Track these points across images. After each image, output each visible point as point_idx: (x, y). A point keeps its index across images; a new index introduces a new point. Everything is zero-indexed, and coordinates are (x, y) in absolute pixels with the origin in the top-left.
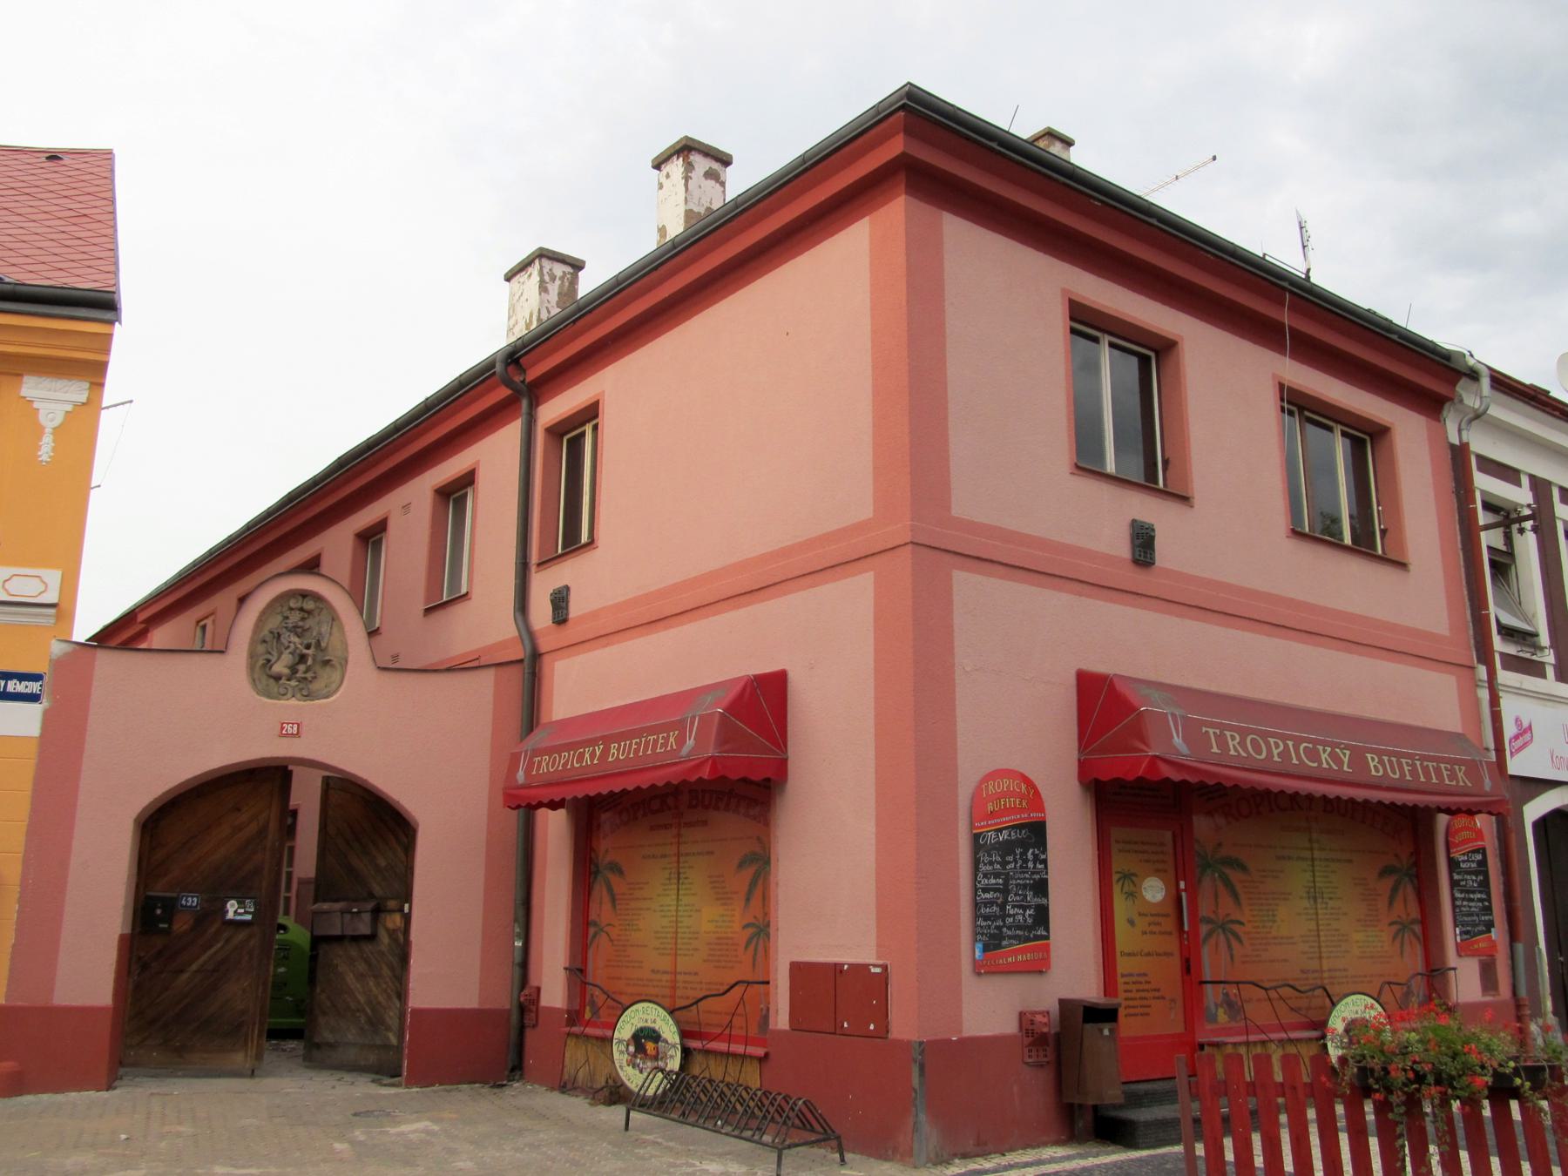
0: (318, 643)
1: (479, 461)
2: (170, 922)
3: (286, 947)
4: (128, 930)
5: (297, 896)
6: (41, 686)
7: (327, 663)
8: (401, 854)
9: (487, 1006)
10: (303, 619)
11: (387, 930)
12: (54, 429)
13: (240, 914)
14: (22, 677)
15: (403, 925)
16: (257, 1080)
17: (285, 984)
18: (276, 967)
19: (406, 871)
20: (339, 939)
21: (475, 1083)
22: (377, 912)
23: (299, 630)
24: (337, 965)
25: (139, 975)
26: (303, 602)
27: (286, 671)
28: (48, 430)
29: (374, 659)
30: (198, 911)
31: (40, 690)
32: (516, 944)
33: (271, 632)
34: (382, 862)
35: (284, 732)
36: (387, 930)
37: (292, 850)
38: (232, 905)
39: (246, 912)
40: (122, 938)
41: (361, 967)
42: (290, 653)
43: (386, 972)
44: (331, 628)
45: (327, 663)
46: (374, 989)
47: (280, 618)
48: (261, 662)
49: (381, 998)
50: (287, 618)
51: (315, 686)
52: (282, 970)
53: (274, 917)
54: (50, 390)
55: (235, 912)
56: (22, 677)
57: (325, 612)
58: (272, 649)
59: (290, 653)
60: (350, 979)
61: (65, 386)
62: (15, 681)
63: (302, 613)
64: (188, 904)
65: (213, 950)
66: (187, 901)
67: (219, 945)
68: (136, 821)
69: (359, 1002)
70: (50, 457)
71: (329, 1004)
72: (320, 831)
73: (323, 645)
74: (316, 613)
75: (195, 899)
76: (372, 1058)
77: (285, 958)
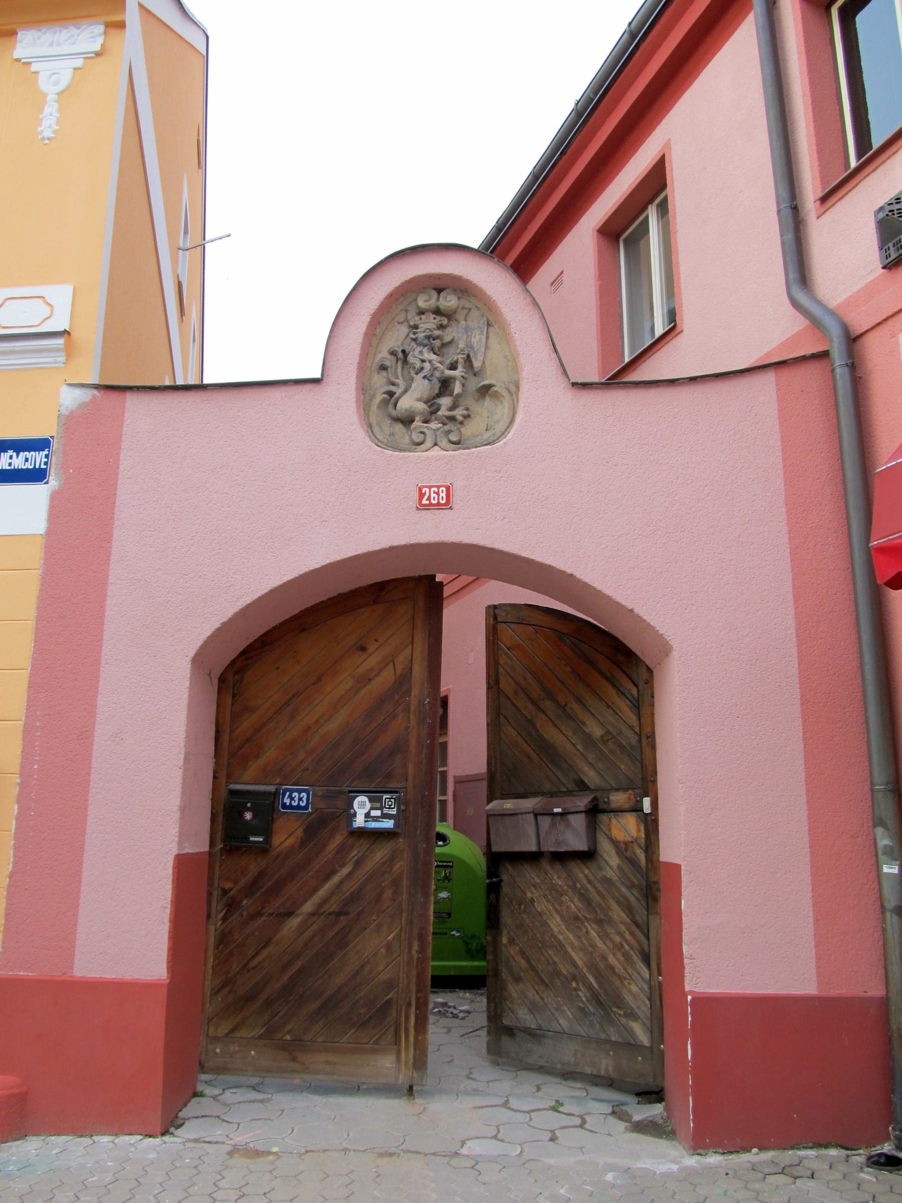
0: (468, 360)
1: (669, 140)
2: (267, 832)
3: (447, 864)
4: (200, 844)
5: (454, 796)
6: (47, 456)
7: (485, 391)
8: (632, 718)
9: (834, 992)
10: (441, 327)
11: (615, 843)
12: (58, 94)
13: (376, 819)
14: (20, 446)
15: (643, 835)
16: (419, 1101)
17: (449, 915)
18: (438, 889)
19: (640, 741)
20: (534, 857)
21: (826, 1146)
22: (594, 811)
23: (437, 343)
24: (532, 901)
25: (224, 919)
26: (438, 299)
27: (421, 406)
28: (52, 97)
29: (565, 372)
30: (310, 814)
31: (46, 463)
32: (886, 869)
33: (393, 353)
34: (597, 732)
35: (424, 501)
36: (615, 843)
37: (444, 746)
38: (362, 805)
39: (385, 816)
40: (183, 863)
41: (574, 905)
42: (424, 377)
43: (618, 913)
44: (487, 338)
45: (485, 391)
46: (600, 943)
47: (404, 329)
48: (379, 397)
49: (612, 960)
50: (416, 327)
51: (469, 429)
52: (444, 895)
53: (430, 824)
54: (51, 45)
55: (367, 815)
56: (20, 446)
57: (475, 313)
58: (397, 378)
59: (424, 377)
60: (556, 923)
61: (72, 36)
62: (10, 452)
63: (438, 318)
64: (294, 804)
65: (336, 879)
66: (292, 799)
67: (345, 871)
68: (199, 660)
69: (574, 964)
70: (54, 132)
71: (523, 963)
72: (489, 688)
73: (477, 364)
74: (460, 316)
75: (304, 795)
76: (605, 1064)
77: (447, 878)
